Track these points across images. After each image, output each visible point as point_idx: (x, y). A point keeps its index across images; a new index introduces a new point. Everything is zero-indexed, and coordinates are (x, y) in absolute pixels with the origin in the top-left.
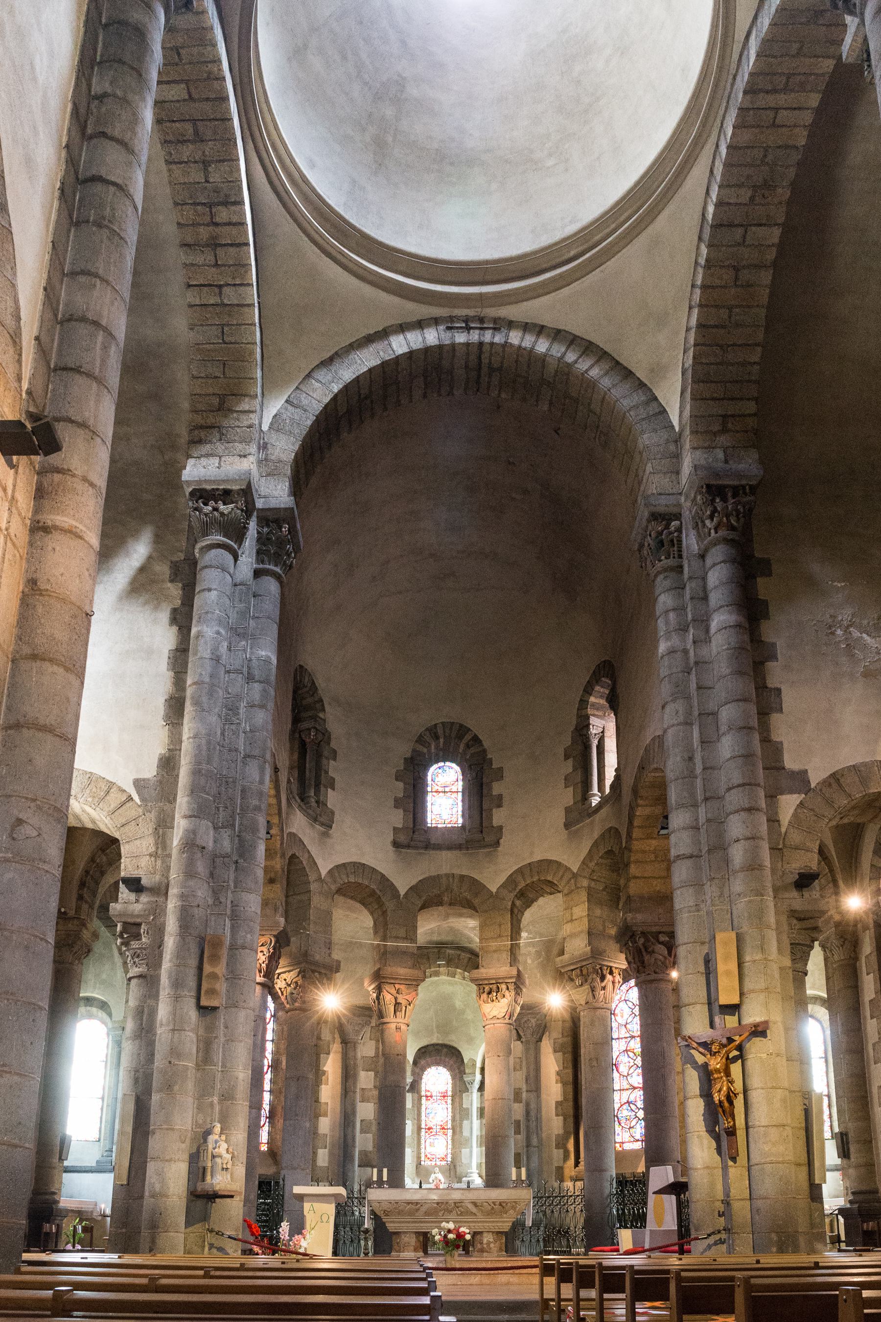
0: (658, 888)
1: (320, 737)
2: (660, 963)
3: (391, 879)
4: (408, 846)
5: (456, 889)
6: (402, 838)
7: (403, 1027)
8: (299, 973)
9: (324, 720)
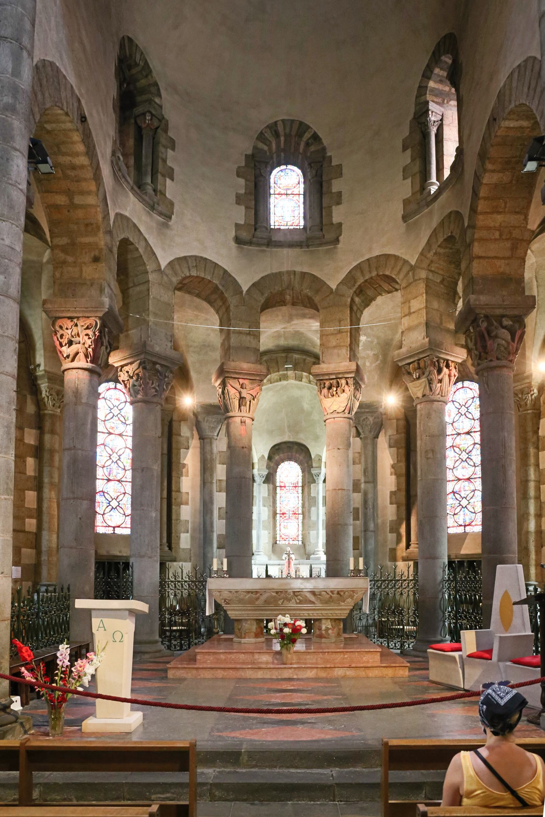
0: (501, 270)
1: (156, 123)
2: (502, 349)
3: (233, 275)
4: (250, 243)
5: (297, 286)
6: (245, 235)
7: (248, 421)
8: (140, 364)
9: (161, 107)
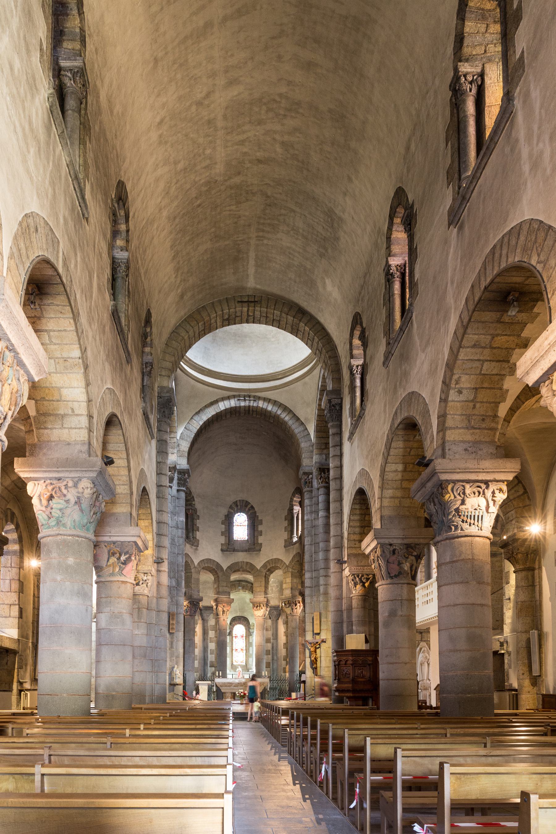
4: (227, 551)
6: (224, 548)
